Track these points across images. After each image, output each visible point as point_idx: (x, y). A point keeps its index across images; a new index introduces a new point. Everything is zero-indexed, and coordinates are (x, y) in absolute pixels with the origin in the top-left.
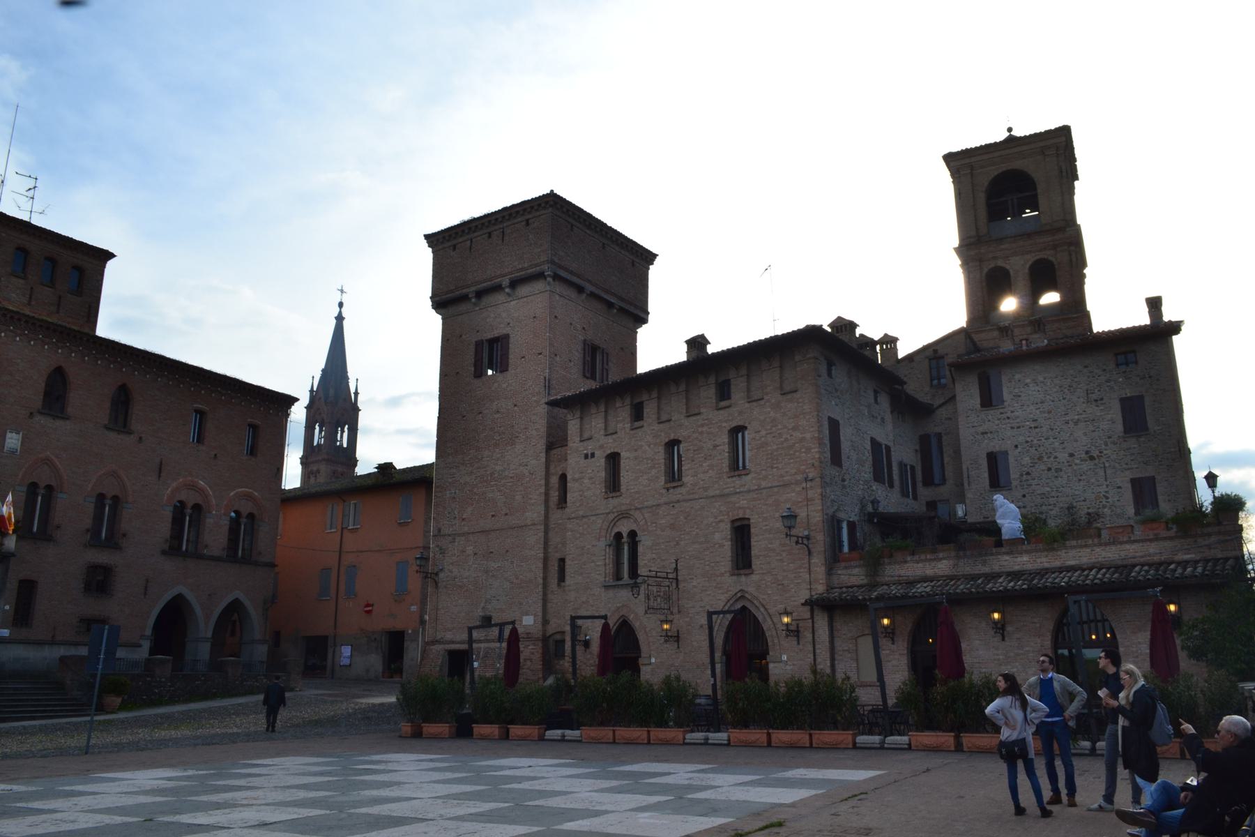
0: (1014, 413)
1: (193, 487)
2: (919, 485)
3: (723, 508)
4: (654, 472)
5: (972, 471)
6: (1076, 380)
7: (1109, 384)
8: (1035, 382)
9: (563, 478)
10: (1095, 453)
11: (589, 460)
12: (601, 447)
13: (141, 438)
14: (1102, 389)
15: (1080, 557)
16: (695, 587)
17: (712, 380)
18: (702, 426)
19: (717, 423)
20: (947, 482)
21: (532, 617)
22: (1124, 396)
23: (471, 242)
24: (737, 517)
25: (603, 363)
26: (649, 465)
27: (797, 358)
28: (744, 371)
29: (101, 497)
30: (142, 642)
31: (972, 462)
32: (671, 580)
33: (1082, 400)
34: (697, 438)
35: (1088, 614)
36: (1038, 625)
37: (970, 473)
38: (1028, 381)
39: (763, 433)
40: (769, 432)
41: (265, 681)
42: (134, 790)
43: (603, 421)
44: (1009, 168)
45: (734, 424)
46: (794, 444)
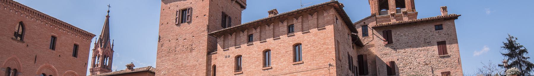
0: (397, 47)
1: (50, 68)
2: (358, 75)
4: (257, 63)
5: (380, 69)
6: (420, 34)
7: (433, 36)
8: (405, 35)
10: (428, 63)
11: (227, 58)
12: (233, 53)
13: (27, 45)
14: (430, 38)
17: (285, 24)
18: (281, 43)
19: (287, 42)
22: (439, 41)
29: (9, 69)
31: (381, 65)
34: (278, 48)
37: (380, 70)
39: (309, 46)
45: (295, 42)
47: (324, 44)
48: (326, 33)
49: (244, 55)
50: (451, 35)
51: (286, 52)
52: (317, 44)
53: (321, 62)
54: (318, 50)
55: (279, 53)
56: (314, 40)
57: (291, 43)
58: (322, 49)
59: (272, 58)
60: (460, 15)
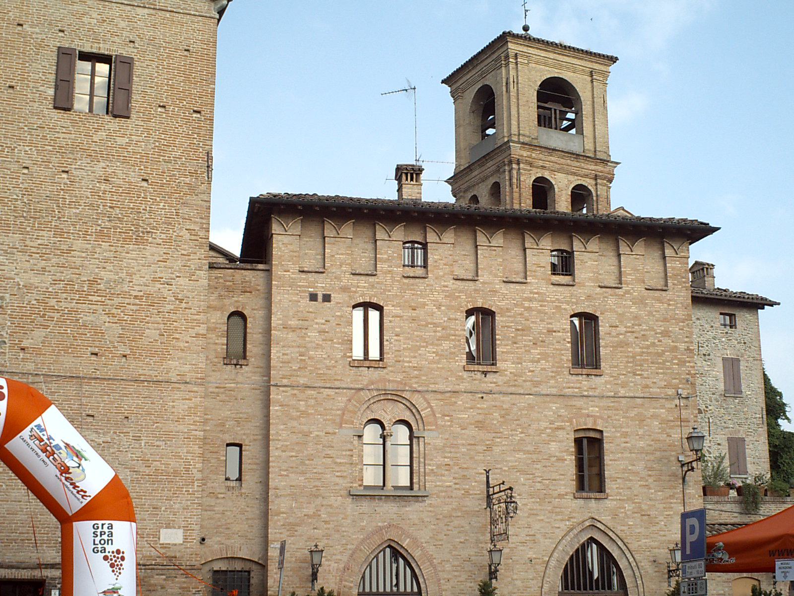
3: (562, 412)
4: (446, 345)
11: (319, 304)
46: (664, 352)
47: (666, 333)
48: (669, 305)
49: (390, 308)
50: (750, 347)
51: (551, 331)
52: (645, 330)
53: (655, 383)
54: (648, 347)
55: (523, 330)
56: (636, 317)
57: (565, 309)
58: (660, 349)
59: (499, 340)
60: (779, 304)
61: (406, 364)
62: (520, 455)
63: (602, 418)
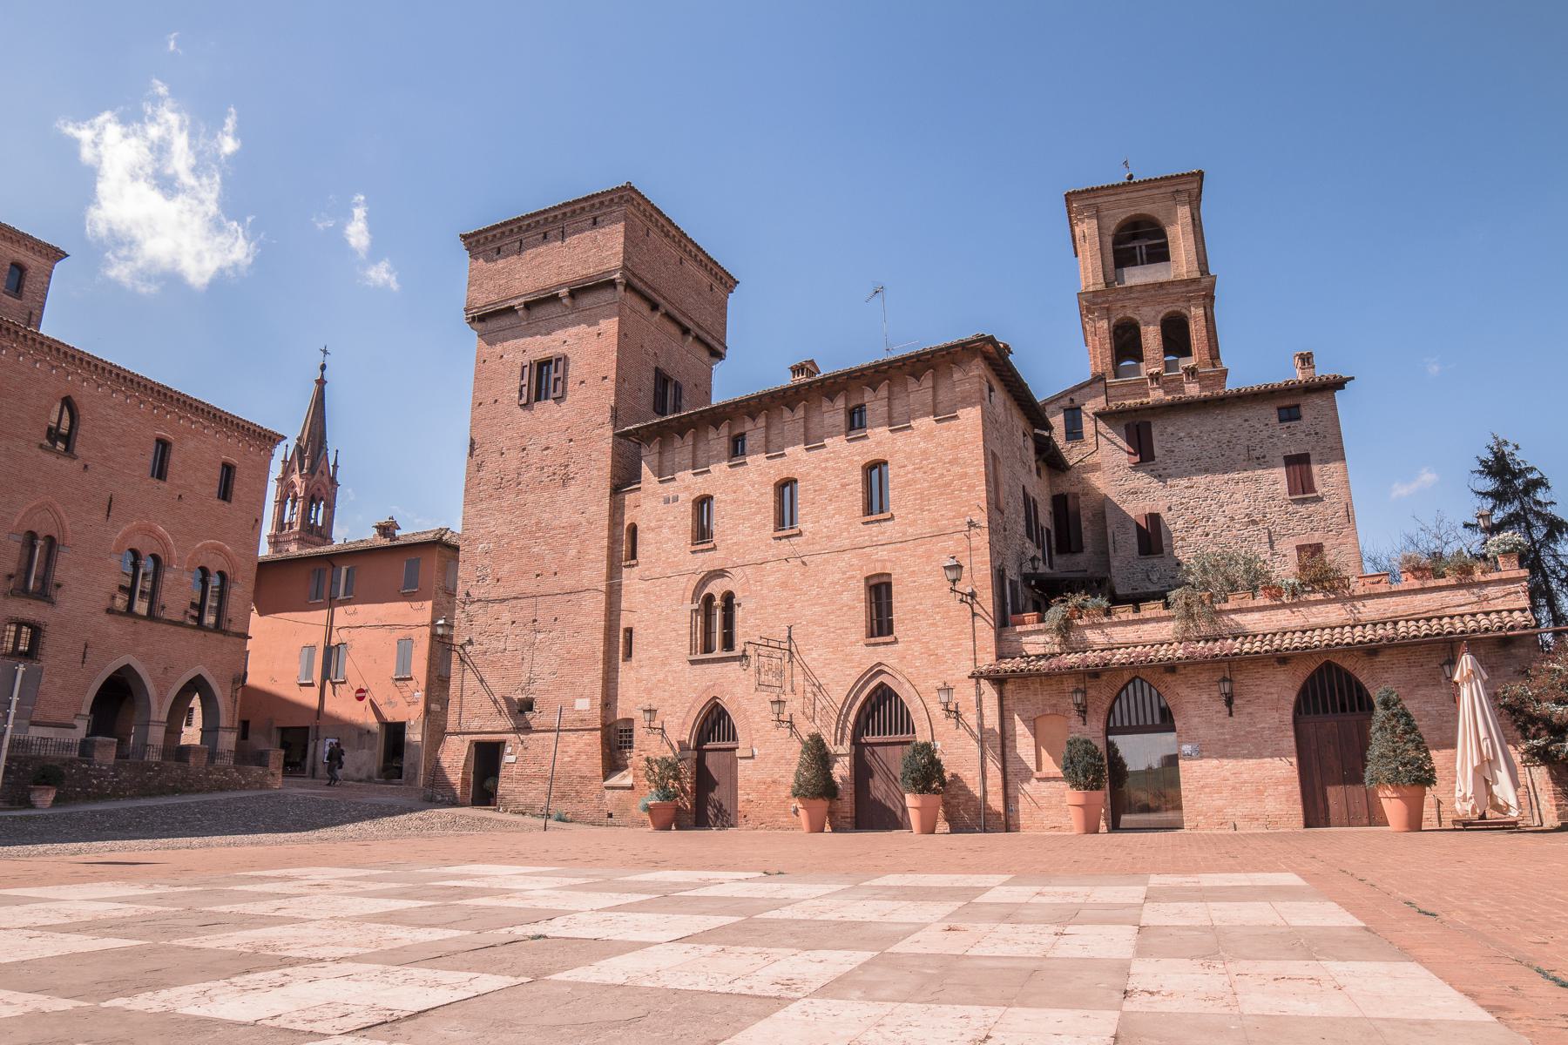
0: (1167, 471)
1: (150, 532)
2: (1054, 552)
3: (855, 561)
4: (759, 517)
6: (1235, 434)
7: (1271, 440)
8: (1189, 435)
9: (633, 529)
11: (671, 505)
12: (687, 488)
15: (1328, 612)
16: (814, 659)
17: (840, 403)
18: (827, 460)
20: (1085, 550)
21: (587, 701)
23: (521, 243)
24: (874, 573)
25: (675, 399)
26: (753, 510)
27: (957, 376)
28: (883, 392)
30: (76, 722)
32: (783, 651)
33: (1242, 457)
34: (819, 475)
35: (1153, 720)
36: (1276, 696)
38: (1182, 435)
39: (910, 467)
40: (917, 466)
41: (236, 774)
42: (58, 922)
43: (691, 456)
44: (1138, 212)
46: (952, 481)
50: (1325, 437)
52: (933, 463)
55: (821, 490)
56: (924, 451)
60: (1353, 378)
61: (729, 542)
62: (817, 609)
63: (890, 561)
